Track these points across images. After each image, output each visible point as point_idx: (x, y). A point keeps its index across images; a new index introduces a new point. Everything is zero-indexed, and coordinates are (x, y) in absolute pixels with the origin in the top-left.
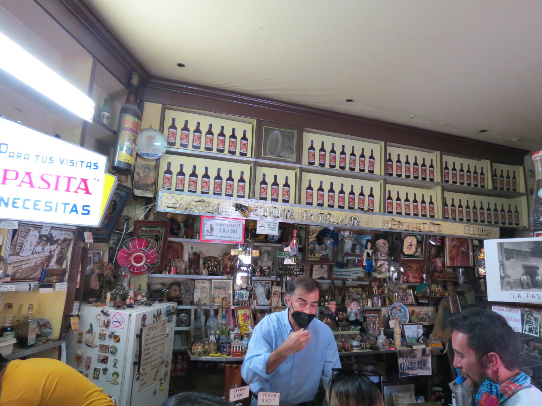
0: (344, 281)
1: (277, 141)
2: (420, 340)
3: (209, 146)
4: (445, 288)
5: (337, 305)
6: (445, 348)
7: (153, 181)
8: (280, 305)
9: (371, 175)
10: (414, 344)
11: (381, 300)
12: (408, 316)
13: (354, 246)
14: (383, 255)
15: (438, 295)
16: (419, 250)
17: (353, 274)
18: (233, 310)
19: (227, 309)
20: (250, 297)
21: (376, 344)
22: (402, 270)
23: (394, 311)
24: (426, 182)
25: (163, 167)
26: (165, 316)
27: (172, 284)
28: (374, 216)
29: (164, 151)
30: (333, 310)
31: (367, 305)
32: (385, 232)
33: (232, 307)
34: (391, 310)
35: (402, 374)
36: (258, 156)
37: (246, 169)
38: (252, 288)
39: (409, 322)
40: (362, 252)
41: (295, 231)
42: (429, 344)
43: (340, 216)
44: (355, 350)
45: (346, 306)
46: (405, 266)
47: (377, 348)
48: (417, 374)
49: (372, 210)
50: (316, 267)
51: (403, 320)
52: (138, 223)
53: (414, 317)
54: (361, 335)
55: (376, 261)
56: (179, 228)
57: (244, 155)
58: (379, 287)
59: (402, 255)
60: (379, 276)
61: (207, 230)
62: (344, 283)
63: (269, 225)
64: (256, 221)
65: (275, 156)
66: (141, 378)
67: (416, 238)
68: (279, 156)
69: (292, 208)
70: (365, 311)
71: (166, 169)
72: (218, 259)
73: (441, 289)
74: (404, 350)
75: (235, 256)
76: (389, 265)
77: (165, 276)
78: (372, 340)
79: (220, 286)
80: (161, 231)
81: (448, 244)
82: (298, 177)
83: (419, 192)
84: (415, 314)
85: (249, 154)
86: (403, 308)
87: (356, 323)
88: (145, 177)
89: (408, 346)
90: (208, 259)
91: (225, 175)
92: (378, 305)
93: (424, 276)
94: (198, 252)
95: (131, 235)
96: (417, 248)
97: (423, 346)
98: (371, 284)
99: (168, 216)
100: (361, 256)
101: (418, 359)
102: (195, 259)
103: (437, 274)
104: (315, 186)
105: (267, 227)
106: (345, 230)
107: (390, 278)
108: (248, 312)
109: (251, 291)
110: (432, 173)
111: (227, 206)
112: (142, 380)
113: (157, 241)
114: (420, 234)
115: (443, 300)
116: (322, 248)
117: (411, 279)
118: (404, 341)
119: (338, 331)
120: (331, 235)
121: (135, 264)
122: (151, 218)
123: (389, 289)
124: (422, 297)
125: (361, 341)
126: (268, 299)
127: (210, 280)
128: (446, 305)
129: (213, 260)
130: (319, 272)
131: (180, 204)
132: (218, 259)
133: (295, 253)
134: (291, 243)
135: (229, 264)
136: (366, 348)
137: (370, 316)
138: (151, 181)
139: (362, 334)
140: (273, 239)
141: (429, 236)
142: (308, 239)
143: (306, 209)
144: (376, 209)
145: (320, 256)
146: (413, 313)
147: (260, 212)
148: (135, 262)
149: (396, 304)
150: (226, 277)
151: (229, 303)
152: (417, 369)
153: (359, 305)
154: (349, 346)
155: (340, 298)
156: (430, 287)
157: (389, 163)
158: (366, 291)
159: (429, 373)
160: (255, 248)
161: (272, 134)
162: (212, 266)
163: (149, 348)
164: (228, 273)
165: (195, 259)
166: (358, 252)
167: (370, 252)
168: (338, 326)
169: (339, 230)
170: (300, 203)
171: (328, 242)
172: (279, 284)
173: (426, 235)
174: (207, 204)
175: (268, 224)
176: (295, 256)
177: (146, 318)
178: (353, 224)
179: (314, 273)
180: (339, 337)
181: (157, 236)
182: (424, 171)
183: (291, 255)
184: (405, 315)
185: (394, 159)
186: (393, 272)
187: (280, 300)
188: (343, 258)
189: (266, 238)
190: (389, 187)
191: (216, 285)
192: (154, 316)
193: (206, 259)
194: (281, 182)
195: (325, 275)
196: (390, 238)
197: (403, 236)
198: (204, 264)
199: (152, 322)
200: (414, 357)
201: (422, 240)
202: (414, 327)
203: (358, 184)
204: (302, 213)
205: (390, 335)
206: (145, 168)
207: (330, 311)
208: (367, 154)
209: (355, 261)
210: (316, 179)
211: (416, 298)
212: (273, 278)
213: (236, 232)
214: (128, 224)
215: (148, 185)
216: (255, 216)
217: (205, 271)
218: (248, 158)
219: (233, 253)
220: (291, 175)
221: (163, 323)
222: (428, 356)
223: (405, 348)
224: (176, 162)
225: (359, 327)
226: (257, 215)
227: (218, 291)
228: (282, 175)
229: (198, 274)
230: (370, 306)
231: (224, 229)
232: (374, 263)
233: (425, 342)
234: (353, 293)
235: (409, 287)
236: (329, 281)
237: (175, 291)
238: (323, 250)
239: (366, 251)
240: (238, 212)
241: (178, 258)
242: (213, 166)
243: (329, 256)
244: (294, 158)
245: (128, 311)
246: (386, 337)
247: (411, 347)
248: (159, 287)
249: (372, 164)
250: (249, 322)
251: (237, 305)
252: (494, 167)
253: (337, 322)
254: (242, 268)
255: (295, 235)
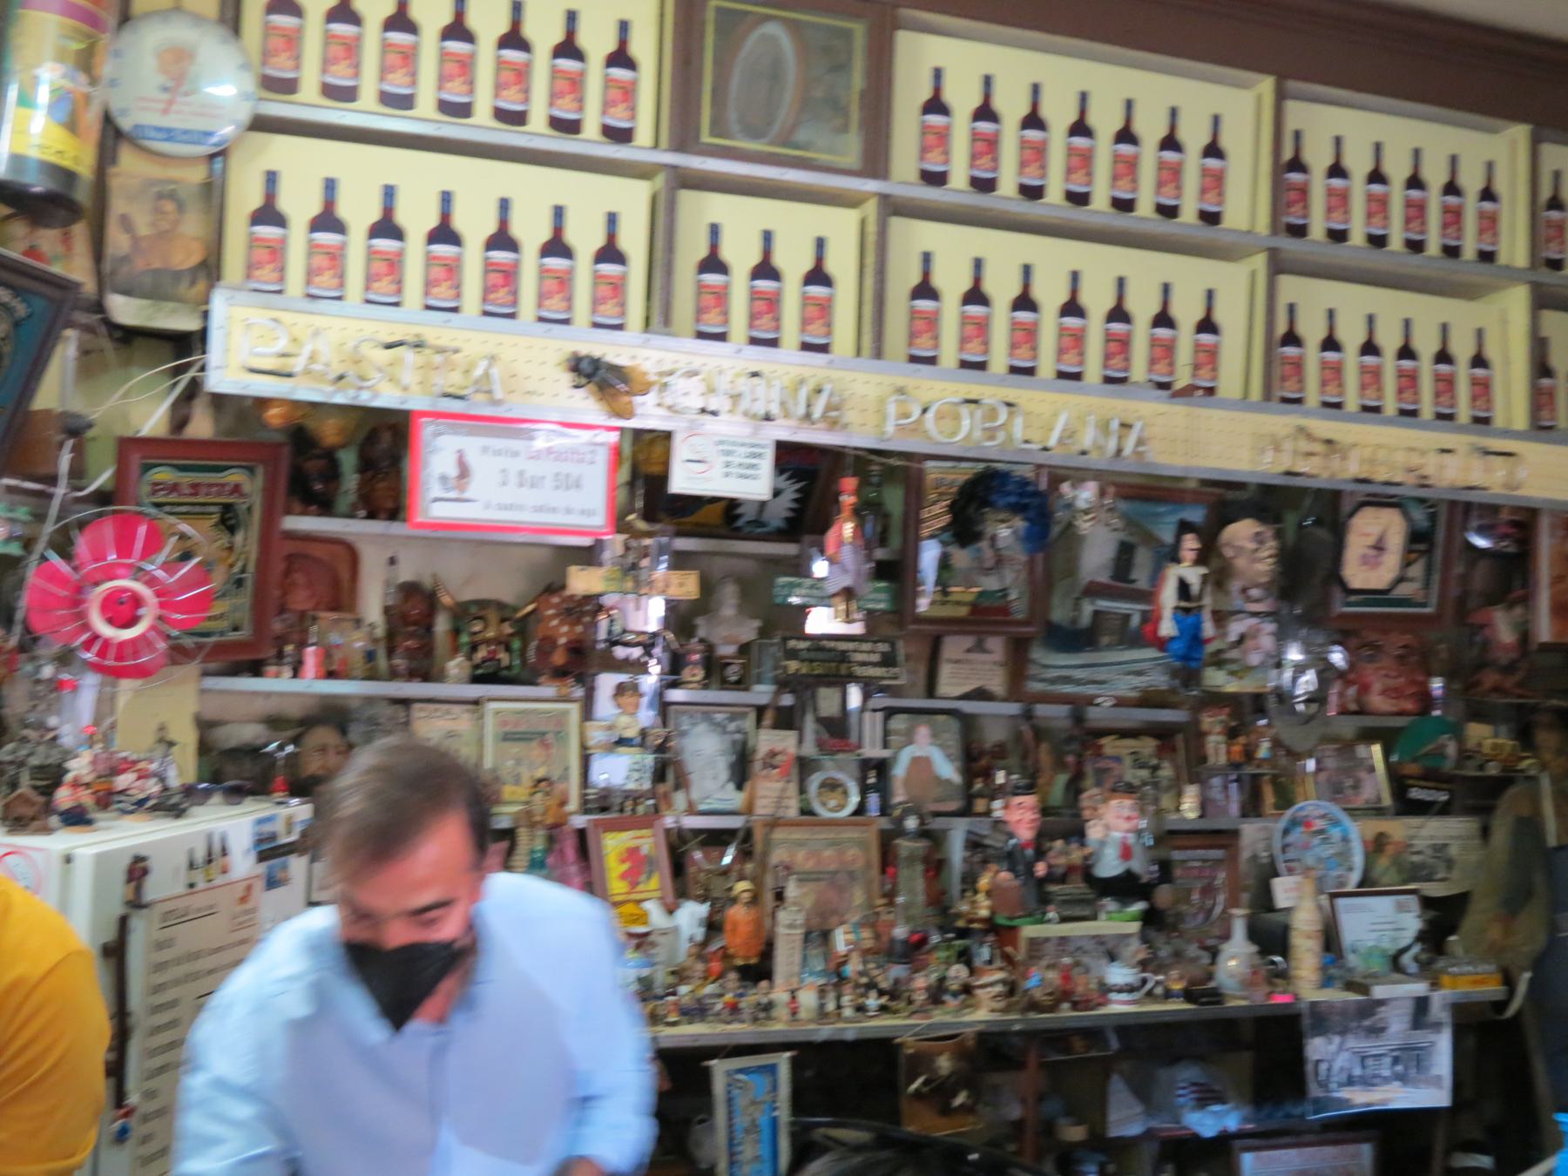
0: (1078, 706)
1: (775, 74)
2: (1406, 959)
3: (340, 78)
4: (1525, 736)
5: (1045, 811)
6: (1511, 992)
7: (195, 258)
8: (792, 812)
9: (1207, 233)
10: (1376, 978)
11: (1241, 788)
12: (1358, 860)
13: (1125, 553)
14: (1255, 592)
15: (1493, 770)
16: (1417, 570)
17: (1116, 679)
18: (581, 834)
19: (554, 832)
20: (659, 775)
21: (1210, 977)
22: (1337, 657)
23: (1297, 835)
24: (1458, 271)
25: (245, 195)
26: (253, 857)
27: (307, 723)
28: (1217, 414)
29: (244, 114)
30: (1025, 833)
31: (1178, 810)
32: (1267, 490)
33: (580, 821)
34: (1286, 832)
35: (1320, 1105)
36: (684, 139)
37: (632, 201)
38: (667, 739)
39: (1361, 884)
40: (1157, 577)
41: (850, 483)
42: (1445, 979)
43: (1056, 415)
44: (1119, 1006)
45: (1087, 814)
46: (1354, 642)
47: (1216, 996)
48: (1385, 1102)
49: (1210, 391)
50: (954, 647)
51: (1335, 873)
52: (129, 446)
53: (1383, 862)
54: (1145, 939)
55: (1220, 618)
56: (332, 473)
57: (620, 135)
58: (1232, 734)
59: (1338, 595)
60: (1232, 686)
61: (444, 479)
62: (1078, 718)
63: (728, 453)
64: (667, 436)
65: (771, 143)
66: (138, 1129)
67: (1406, 515)
68: (786, 143)
69: (835, 374)
70: (1168, 837)
71: (255, 201)
72: (516, 609)
73: (1507, 743)
74: (1330, 1005)
75: (588, 598)
76: (1282, 637)
77: (277, 684)
78: (1194, 960)
79: (522, 729)
80: (247, 488)
81: (1546, 545)
82: (871, 238)
83: (1427, 315)
84: (1390, 849)
85: (644, 135)
86: (1336, 823)
87: (1125, 888)
88: (163, 236)
89: (1350, 986)
90: (473, 610)
91: (531, 231)
92: (1224, 811)
93: (1437, 685)
94: (427, 582)
95: (103, 498)
96: (1407, 564)
97: (1419, 988)
98: (1196, 722)
99: (274, 415)
100: (1149, 596)
101: (1396, 1042)
102: (415, 609)
103: (1490, 678)
104: (952, 281)
105: (722, 461)
106: (1079, 475)
107: (1283, 697)
108: (648, 842)
109: (661, 749)
110: (1489, 223)
111: (528, 360)
112: (145, 1140)
113: (232, 530)
114: (1422, 501)
115: (1512, 791)
116: (979, 559)
117: (1377, 701)
118: (1333, 962)
119: (1042, 922)
120: (1012, 499)
121: (107, 631)
122: (202, 426)
123: (1277, 743)
124: (1425, 777)
125: (1144, 965)
126: (739, 787)
127: (476, 702)
128: (1525, 811)
129: (493, 616)
130: (968, 671)
131: (312, 358)
132: (516, 609)
133: (847, 581)
134: (831, 536)
135: (564, 633)
136: (1168, 995)
137: (1186, 857)
138: (186, 256)
139: (1152, 934)
140: (758, 523)
141: (1465, 509)
142: (919, 522)
143: (900, 381)
144: (1230, 379)
145: (969, 598)
146: (1377, 845)
147: (689, 394)
148: (112, 622)
149: (1311, 805)
150: (548, 690)
151: (563, 803)
152: (1387, 1080)
153: (1143, 812)
154: (1093, 986)
155: (1062, 779)
156: (1457, 732)
157: (1295, 177)
158: (1174, 749)
159: (1433, 1094)
160: (680, 561)
161: (755, 36)
162: (488, 642)
163: (172, 1004)
164: (560, 674)
165: (415, 609)
166: (1140, 576)
167: (1194, 575)
168: (1044, 900)
169: (1057, 477)
170: (878, 353)
171: (1005, 531)
172: (786, 720)
173: (1453, 504)
174: (438, 359)
175: (726, 446)
176: (848, 593)
177: (145, 872)
178: (1119, 451)
179: (945, 671)
180: (1050, 948)
181: (227, 508)
182: (1453, 217)
183: (833, 587)
184: (1344, 855)
185: (1318, 158)
186: (1300, 669)
187: (793, 788)
188: (1077, 606)
189: (725, 517)
190: (1291, 288)
191: (505, 723)
192: (192, 866)
193: (464, 613)
194: (793, 261)
195: (996, 682)
196: (1290, 520)
197: (1346, 507)
198: (456, 632)
199: (181, 889)
200: (1377, 1031)
201: (1435, 523)
202: (1382, 906)
203: (1146, 274)
204: (882, 401)
205: (1272, 939)
206: (160, 196)
207: (1011, 835)
208: (1194, 137)
209: (1127, 617)
210: (952, 251)
211: (1399, 784)
212: (762, 693)
213: (578, 485)
214: (78, 451)
215: (177, 276)
216: (662, 412)
217: (456, 666)
218: (641, 149)
219: (582, 581)
220: (842, 230)
221: (239, 891)
222: (1437, 1026)
223: (1336, 996)
224: (301, 168)
225: (1139, 907)
226: (670, 408)
227: (515, 749)
228: (796, 230)
229: (426, 678)
230: (1192, 815)
231: (521, 474)
232: (1208, 629)
233: (1426, 970)
234: (1118, 759)
235: (1369, 736)
236: (1013, 708)
237: (323, 749)
238: (987, 571)
239: (1173, 574)
240: (581, 393)
241: (335, 606)
242: (478, 190)
243: (1013, 595)
244: (850, 149)
245: (63, 841)
246: (1254, 948)
247: (1363, 989)
248: (249, 733)
249: (1214, 183)
250: (654, 883)
251: (604, 809)
252: (1290, 125)
253: (1042, 882)
254: (620, 652)
255: (848, 500)
